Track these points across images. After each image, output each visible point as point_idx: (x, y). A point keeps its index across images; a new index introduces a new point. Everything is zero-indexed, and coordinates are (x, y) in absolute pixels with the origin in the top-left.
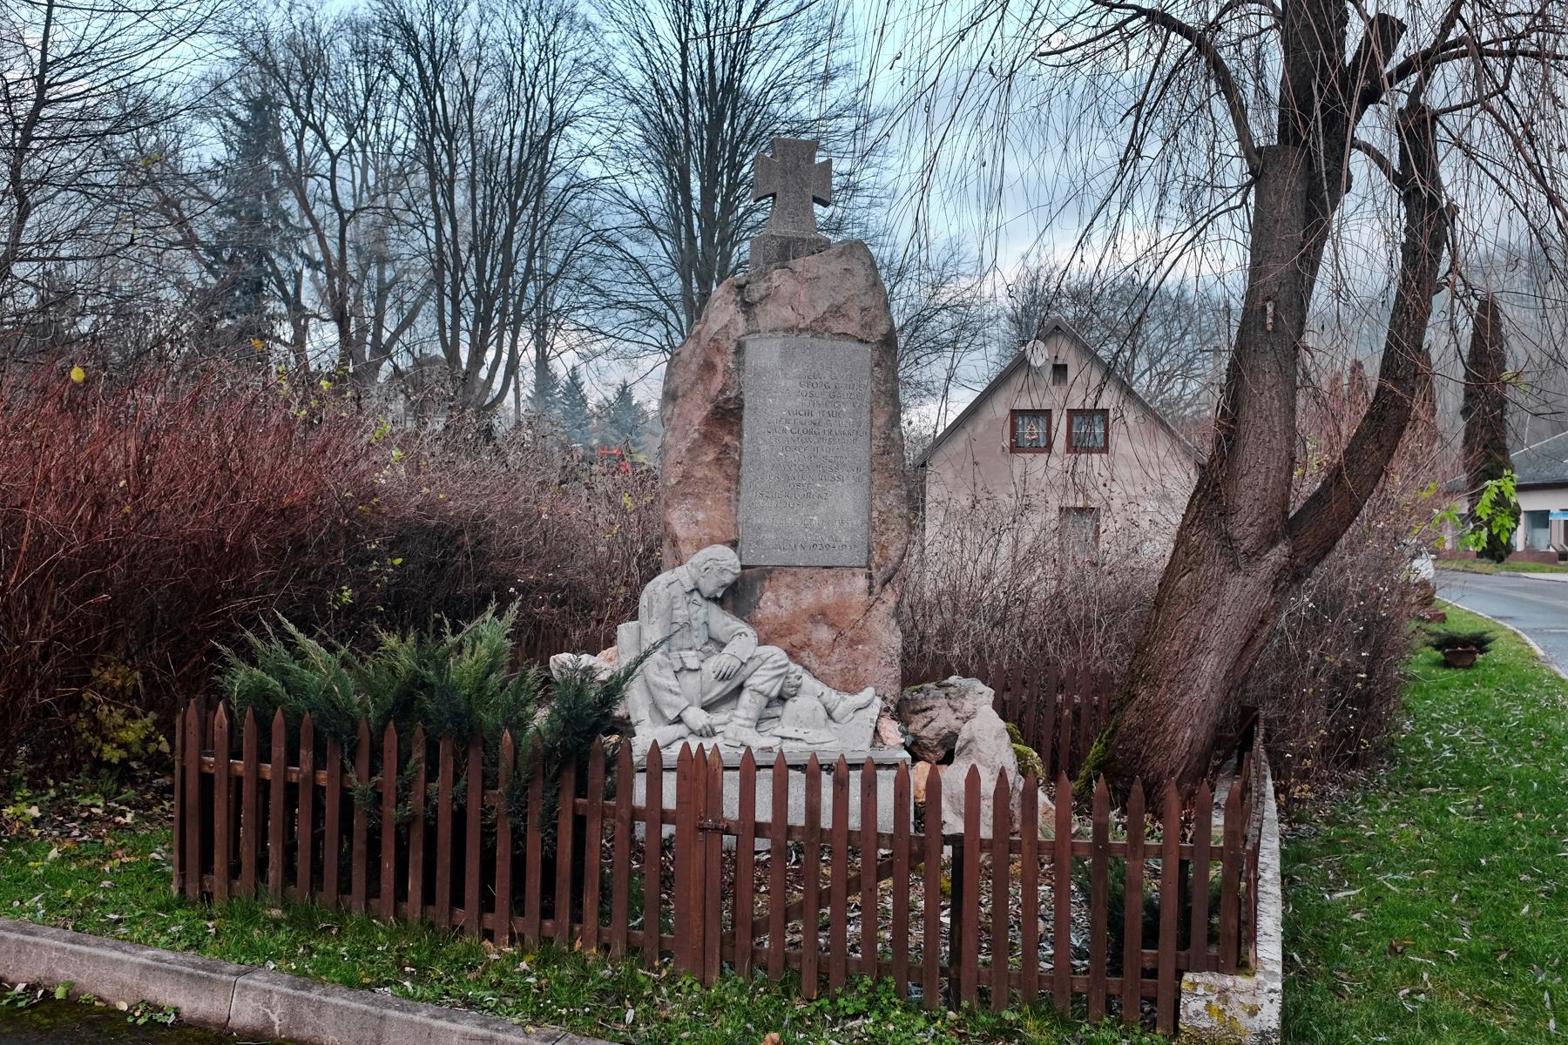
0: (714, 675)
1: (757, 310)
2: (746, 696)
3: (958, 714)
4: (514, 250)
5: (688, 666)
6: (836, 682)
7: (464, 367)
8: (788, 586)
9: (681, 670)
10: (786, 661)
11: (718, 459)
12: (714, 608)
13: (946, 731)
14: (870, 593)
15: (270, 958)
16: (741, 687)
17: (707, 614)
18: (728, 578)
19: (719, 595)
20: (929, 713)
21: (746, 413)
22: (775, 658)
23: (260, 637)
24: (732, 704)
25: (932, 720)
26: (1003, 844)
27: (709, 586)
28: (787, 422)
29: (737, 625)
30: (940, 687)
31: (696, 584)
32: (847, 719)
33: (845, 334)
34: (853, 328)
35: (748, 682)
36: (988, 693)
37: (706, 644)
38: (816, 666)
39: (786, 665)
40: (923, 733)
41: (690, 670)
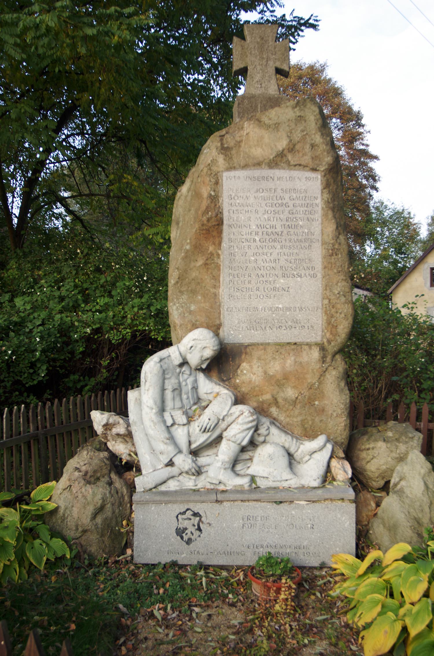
1: (234, 152)
4: (10, 207)
6: (298, 431)
7: (15, 221)
8: (259, 359)
11: (206, 264)
14: (324, 362)
15: (371, 264)
16: (220, 438)
19: (204, 366)
21: (225, 227)
24: (214, 450)
26: (332, 604)
27: (194, 359)
28: (257, 234)
29: (217, 388)
33: (300, 165)
34: (306, 159)
35: (225, 434)
38: (282, 418)
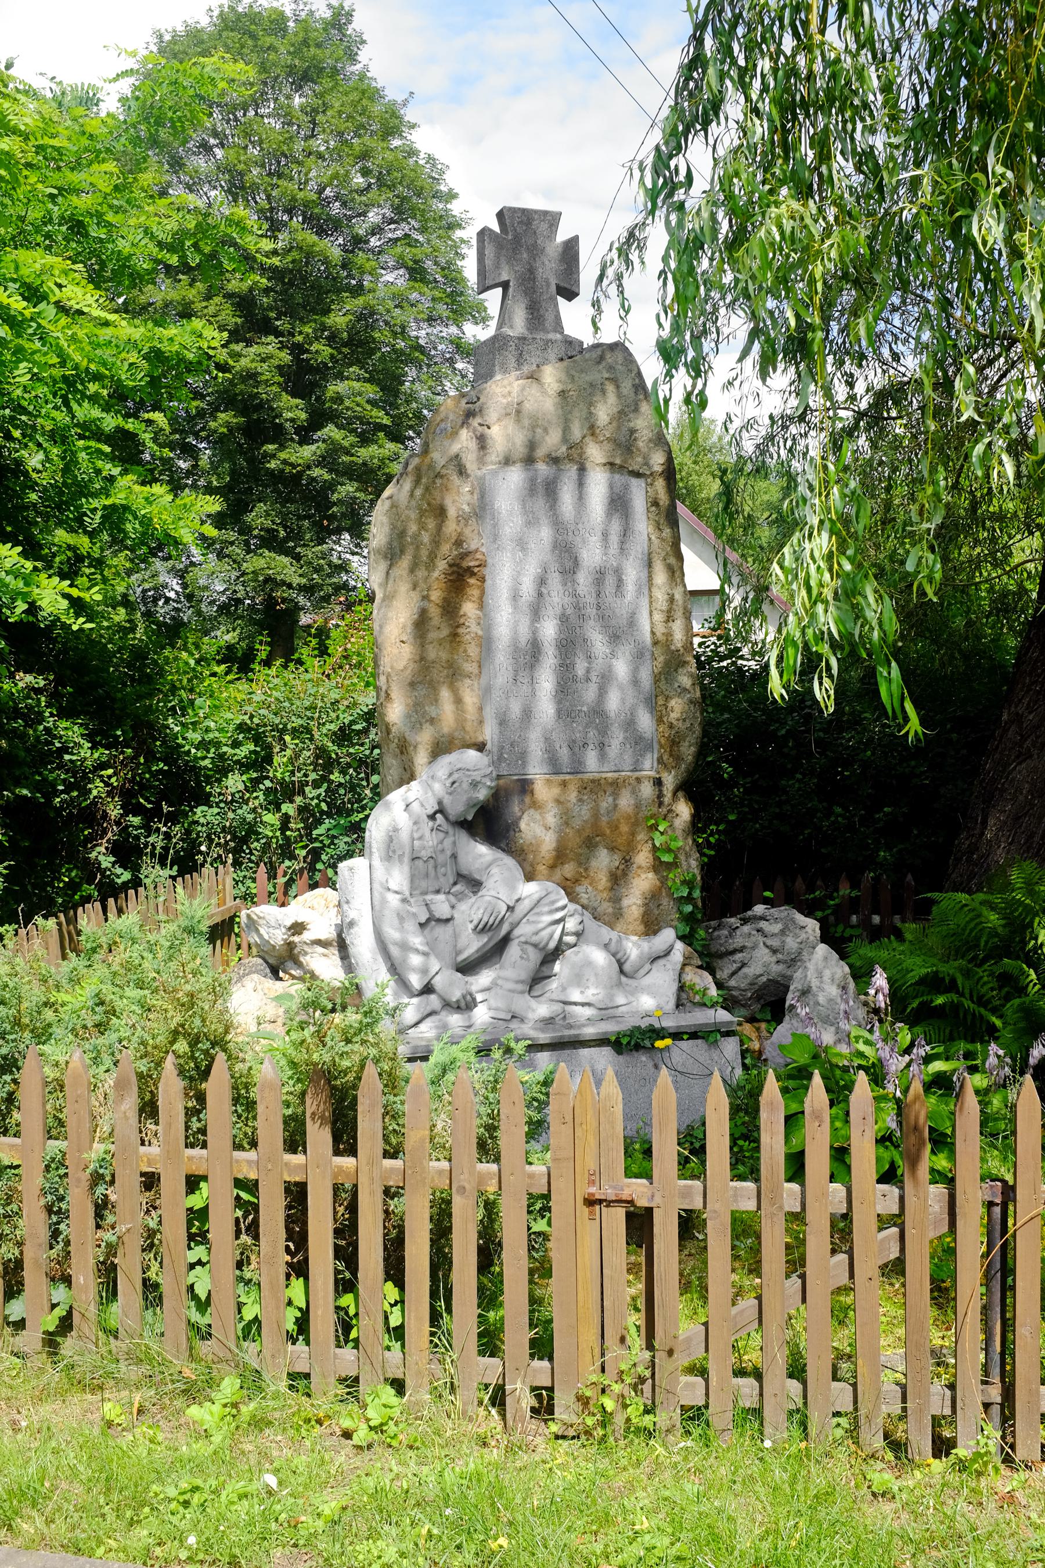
0: (471, 926)
2: (513, 951)
3: (780, 956)
5: (437, 915)
9: (428, 920)
10: (564, 901)
12: (463, 837)
13: (764, 979)
16: (506, 940)
17: (454, 843)
18: (482, 794)
19: (470, 818)
20: (738, 956)
22: (552, 897)
23: (1013, 96)
25: (744, 965)
30: (745, 921)
31: (440, 803)
32: (642, 972)
35: (516, 932)
36: (812, 926)
37: (455, 884)
39: (564, 907)
40: (732, 983)
41: (439, 921)
